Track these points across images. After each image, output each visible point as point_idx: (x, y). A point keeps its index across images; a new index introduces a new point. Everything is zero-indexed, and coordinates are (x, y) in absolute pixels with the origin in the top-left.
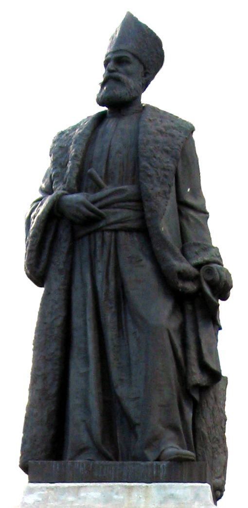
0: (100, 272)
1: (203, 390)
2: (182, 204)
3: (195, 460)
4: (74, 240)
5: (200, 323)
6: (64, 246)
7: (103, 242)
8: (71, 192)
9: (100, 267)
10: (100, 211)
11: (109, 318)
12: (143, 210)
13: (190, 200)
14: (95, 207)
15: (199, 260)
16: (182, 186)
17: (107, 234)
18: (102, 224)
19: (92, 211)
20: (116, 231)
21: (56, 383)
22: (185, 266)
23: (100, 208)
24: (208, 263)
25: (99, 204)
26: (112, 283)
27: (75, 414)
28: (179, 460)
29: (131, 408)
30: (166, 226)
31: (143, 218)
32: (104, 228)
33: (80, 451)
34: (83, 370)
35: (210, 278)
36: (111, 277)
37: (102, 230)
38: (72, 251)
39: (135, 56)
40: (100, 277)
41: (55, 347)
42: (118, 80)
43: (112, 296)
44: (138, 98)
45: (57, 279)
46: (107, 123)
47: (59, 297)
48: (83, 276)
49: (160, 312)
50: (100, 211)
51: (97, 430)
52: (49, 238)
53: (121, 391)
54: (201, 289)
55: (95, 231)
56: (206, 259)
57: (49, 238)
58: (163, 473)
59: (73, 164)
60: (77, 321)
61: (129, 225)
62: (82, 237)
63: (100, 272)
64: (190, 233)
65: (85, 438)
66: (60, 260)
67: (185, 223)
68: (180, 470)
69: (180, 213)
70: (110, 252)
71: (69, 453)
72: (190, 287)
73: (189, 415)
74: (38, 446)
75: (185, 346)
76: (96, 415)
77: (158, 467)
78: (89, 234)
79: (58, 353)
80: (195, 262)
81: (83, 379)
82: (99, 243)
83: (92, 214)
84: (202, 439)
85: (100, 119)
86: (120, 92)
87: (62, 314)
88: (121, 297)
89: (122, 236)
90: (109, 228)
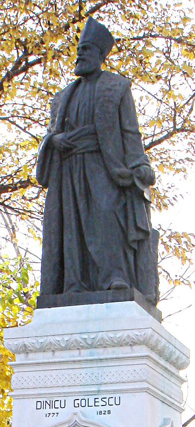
1: (140, 242)
4: (62, 160)
5: (135, 202)
6: (56, 165)
7: (76, 160)
8: (58, 132)
9: (76, 176)
10: (73, 143)
11: (82, 205)
12: (97, 140)
13: (128, 128)
14: (70, 141)
15: (134, 164)
16: (123, 119)
17: (78, 156)
18: (74, 151)
19: (68, 144)
20: (84, 153)
21: (57, 246)
22: (124, 170)
23: (72, 141)
24: (139, 165)
25: (71, 140)
26: (83, 186)
27: (67, 263)
29: (95, 257)
30: (111, 149)
31: (98, 144)
32: (77, 152)
34: (70, 236)
35: (138, 175)
36: (82, 181)
37: (76, 154)
39: (93, 43)
40: (76, 181)
41: (55, 225)
42: (83, 60)
45: (53, 184)
46: (53, 112)
47: (55, 197)
48: (66, 181)
50: (73, 143)
52: (48, 161)
53: (91, 249)
55: (71, 155)
56: (138, 163)
57: (48, 161)
58: (110, 298)
59: (59, 115)
60: (65, 208)
61: (91, 149)
62: (65, 158)
64: (129, 147)
65: (73, 279)
66: (54, 174)
67: (125, 142)
69: (122, 135)
72: (127, 182)
73: (131, 257)
74: (49, 284)
75: (126, 218)
76: (77, 262)
77: (107, 294)
78: (69, 157)
80: (131, 166)
82: (74, 161)
83: (68, 146)
84: (6, 320)
85: (78, 83)
86: (86, 68)
87: (58, 205)
88: (88, 192)
89: (86, 155)
90: (78, 152)
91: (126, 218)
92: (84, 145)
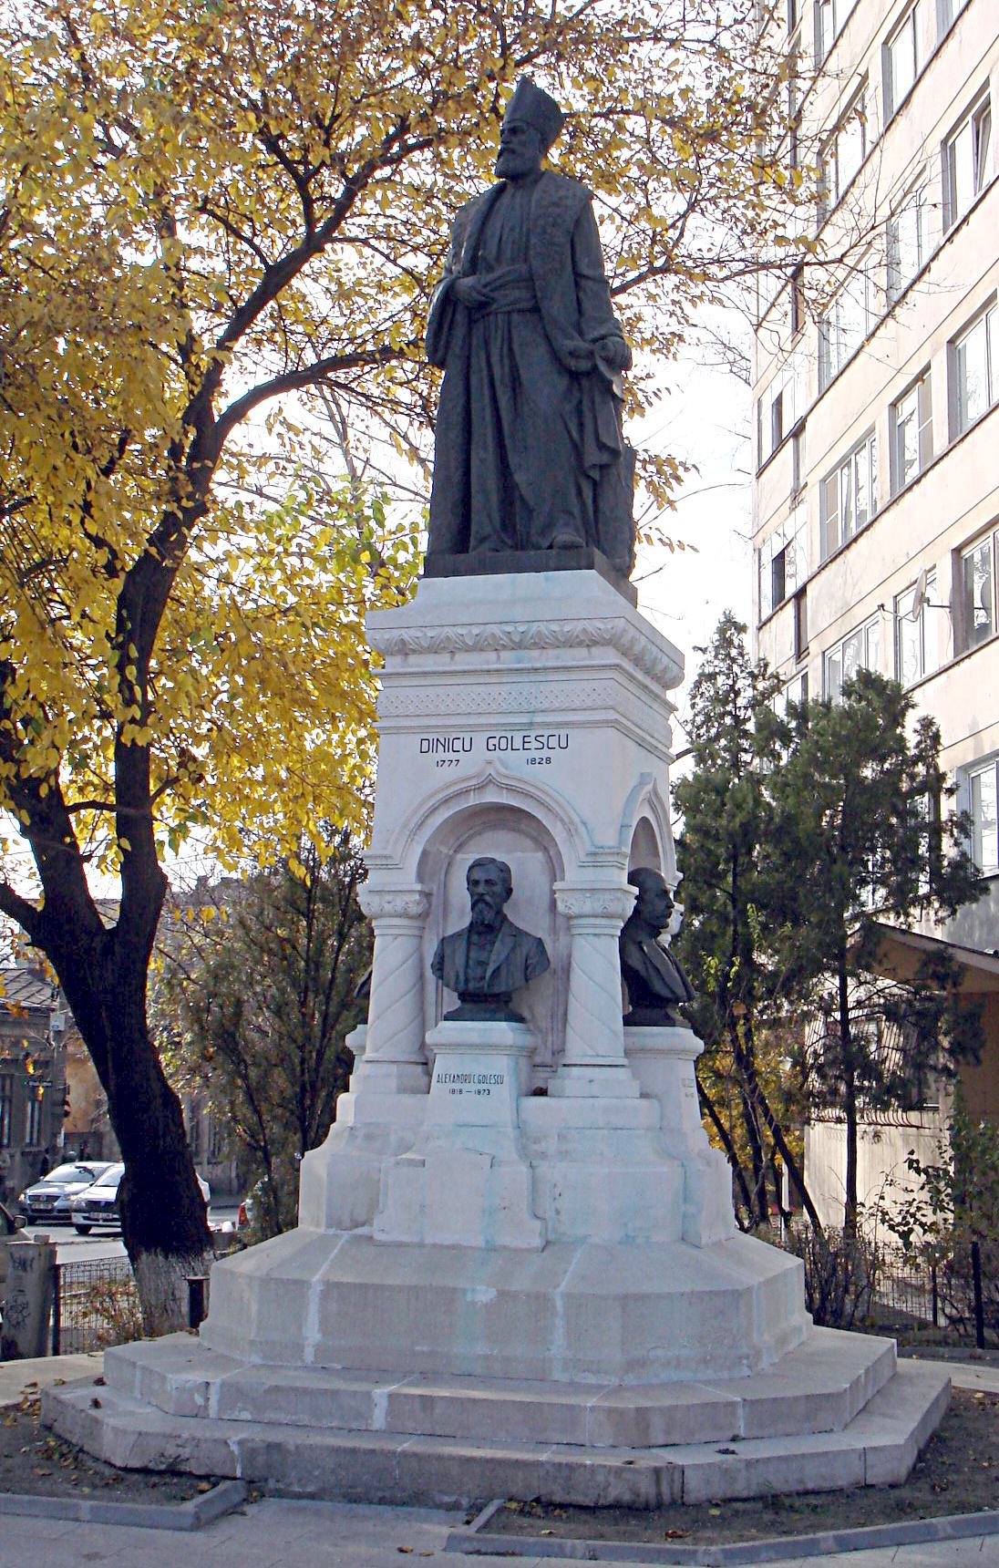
0: (988, 824)
2: (578, 275)
3: (580, 540)
4: (471, 322)
6: (460, 332)
13: (586, 271)
15: (596, 334)
26: (507, 369)
28: (568, 547)
29: (525, 490)
30: (557, 306)
33: (483, 540)
36: (506, 361)
38: (469, 333)
40: (495, 360)
43: (507, 380)
44: (536, 162)
48: (478, 362)
49: (545, 387)
51: (496, 516)
54: (595, 368)
63: (988, 824)
67: (582, 295)
68: (570, 557)
69: (577, 284)
70: (496, 410)
71: (473, 542)
72: (584, 365)
75: (581, 425)
76: (494, 499)
79: (459, 441)
81: (484, 458)
85: (500, 190)
86: (516, 165)
87: (462, 401)
91: (581, 425)
92: (511, 298)
